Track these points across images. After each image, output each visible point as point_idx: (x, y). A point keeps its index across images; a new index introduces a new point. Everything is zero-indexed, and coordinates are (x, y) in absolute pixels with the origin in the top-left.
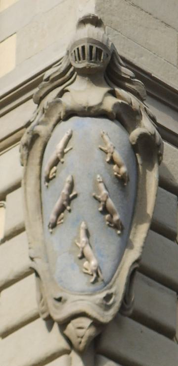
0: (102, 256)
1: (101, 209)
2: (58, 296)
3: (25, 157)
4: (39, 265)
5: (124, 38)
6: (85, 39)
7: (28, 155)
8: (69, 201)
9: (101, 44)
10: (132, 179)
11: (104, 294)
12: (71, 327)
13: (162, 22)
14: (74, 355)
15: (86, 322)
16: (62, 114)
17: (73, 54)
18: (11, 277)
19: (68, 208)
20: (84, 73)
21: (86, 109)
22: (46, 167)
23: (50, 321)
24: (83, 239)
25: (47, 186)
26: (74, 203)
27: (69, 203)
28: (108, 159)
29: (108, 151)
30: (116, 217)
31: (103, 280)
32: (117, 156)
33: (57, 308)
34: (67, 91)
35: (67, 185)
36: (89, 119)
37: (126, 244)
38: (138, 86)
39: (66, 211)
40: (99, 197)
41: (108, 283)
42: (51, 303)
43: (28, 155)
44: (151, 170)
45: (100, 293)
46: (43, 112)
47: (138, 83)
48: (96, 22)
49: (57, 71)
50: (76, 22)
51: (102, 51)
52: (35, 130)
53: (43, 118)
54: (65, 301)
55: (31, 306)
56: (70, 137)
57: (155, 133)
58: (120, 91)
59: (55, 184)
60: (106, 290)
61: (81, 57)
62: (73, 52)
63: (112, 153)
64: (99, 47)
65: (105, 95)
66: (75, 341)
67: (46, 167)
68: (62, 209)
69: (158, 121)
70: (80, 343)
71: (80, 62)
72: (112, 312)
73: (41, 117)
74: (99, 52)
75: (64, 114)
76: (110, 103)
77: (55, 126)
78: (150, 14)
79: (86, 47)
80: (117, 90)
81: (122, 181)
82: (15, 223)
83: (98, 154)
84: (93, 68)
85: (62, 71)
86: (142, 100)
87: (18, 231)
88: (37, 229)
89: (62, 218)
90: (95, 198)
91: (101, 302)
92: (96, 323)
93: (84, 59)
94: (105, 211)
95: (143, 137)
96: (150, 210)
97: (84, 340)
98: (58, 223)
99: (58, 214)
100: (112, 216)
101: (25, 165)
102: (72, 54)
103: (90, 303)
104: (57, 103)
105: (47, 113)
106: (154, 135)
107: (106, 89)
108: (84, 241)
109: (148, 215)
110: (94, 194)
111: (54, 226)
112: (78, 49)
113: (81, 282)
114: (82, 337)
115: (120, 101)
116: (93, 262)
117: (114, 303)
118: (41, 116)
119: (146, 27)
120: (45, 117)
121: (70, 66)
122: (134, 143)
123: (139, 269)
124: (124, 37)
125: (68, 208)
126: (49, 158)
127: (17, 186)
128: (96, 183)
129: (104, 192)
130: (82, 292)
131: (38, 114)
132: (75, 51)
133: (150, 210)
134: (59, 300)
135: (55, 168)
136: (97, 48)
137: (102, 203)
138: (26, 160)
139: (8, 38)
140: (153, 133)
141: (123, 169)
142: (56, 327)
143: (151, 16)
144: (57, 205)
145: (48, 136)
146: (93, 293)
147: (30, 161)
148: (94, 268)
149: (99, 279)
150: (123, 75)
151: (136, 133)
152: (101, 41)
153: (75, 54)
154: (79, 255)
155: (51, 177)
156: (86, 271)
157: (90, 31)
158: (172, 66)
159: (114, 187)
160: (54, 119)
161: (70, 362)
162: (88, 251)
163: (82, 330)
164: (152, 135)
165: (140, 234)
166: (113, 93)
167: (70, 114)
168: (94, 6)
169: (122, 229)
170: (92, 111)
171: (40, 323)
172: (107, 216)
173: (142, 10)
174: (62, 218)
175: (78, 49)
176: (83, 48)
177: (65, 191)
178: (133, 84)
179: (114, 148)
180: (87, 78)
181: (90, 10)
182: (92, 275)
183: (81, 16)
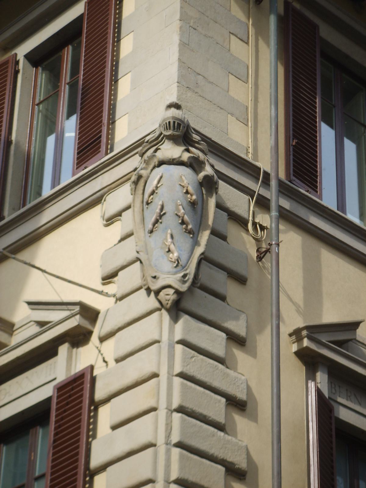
0: (181, 250)
1: (180, 221)
2: (154, 275)
3: (133, 190)
4: (142, 256)
5: (195, 116)
7: (135, 188)
8: (161, 216)
10: (200, 203)
11: (182, 274)
12: (162, 294)
13: (218, 106)
14: (164, 311)
15: (171, 291)
16: (157, 163)
17: (163, 126)
18: (125, 264)
19: (160, 221)
20: (170, 138)
21: (171, 160)
22: (146, 196)
23: (149, 291)
24: (170, 240)
25: (147, 208)
27: (161, 218)
28: (185, 191)
29: (185, 186)
30: (190, 227)
31: (181, 265)
32: (190, 189)
33: (153, 282)
34: (160, 149)
35: (159, 207)
36: (172, 166)
37: (196, 243)
39: (159, 223)
40: (179, 214)
41: (185, 267)
42: (149, 279)
45: (179, 273)
47: (204, 145)
48: (177, 106)
49: (153, 137)
50: (165, 107)
52: (139, 173)
54: (158, 278)
55: (137, 281)
56: (161, 177)
57: (214, 175)
58: (192, 149)
59: (152, 206)
61: (168, 128)
62: (163, 125)
63: (187, 187)
64: (179, 122)
65: (183, 152)
66: (164, 303)
67: (146, 196)
68: (157, 221)
69: (216, 167)
70: (168, 304)
71: (167, 131)
73: (143, 165)
74: (179, 125)
75: (158, 163)
76: (186, 156)
77: (152, 170)
78: (211, 102)
80: (190, 148)
81: (193, 204)
82: (127, 230)
83: (178, 188)
86: (206, 154)
87: (130, 235)
88: (141, 234)
89: (157, 227)
90: (177, 215)
92: (177, 292)
93: (170, 129)
94: (183, 223)
95: (206, 177)
96: (210, 222)
97: (170, 302)
98: (154, 230)
99: (154, 225)
100: (187, 226)
101: (133, 194)
103: (173, 280)
104: (153, 156)
105: (147, 162)
106: (213, 176)
107: (183, 148)
108: (169, 241)
109: (210, 225)
110: (176, 212)
111: (151, 232)
112: (166, 123)
113: (168, 266)
114: (169, 300)
116: (176, 254)
118: (144, 164)
120: (146, 165)
121: (161, 134)
122: (201, 181)
123: (204, 259)
125: (160, 221)
126: (149, 190)
127: (128, 207)
128: (177, 206)
129: (182, 211)
130: (169, 273)
131: (141, 163)
132: (164, 125)
133: (210, 222)
134: (155, 277)
135: (152, 196)
136: (178, 123)
138: (134, 191)
139: (123, 116)
140: (212, 175)
141: (194, 197)
142: (152, 294)
144: (153, 219)
146: (175, 273)
147: (137, 192)
149: (179, 265)
150: (194, 139)
151: (202, 174)
152: (180, 118)
154: (167, 250)
155: (149, 202)
156: (171, 260)
157: (173, 112)
159: (188, 208)
160: (151, 166)
161: (161, 316)
162: (172, 247)
163: (168, 296)
164: (212, 176)
165: (205, 237)
166: (188, 150)
167: (161, 163)
168: (176, 97)
169: (193, 234)
170: (175, 162)
171: (143, 292)
172: (184, 226)
174: (157, 227)
175: (166, 123)
176: (169, 122)
177: (158, 210)
178: (200, 145)
179: (188, 184)
180: (172, 141)
181: (173, 99)
182: (175, 262)
183: (168, 103)
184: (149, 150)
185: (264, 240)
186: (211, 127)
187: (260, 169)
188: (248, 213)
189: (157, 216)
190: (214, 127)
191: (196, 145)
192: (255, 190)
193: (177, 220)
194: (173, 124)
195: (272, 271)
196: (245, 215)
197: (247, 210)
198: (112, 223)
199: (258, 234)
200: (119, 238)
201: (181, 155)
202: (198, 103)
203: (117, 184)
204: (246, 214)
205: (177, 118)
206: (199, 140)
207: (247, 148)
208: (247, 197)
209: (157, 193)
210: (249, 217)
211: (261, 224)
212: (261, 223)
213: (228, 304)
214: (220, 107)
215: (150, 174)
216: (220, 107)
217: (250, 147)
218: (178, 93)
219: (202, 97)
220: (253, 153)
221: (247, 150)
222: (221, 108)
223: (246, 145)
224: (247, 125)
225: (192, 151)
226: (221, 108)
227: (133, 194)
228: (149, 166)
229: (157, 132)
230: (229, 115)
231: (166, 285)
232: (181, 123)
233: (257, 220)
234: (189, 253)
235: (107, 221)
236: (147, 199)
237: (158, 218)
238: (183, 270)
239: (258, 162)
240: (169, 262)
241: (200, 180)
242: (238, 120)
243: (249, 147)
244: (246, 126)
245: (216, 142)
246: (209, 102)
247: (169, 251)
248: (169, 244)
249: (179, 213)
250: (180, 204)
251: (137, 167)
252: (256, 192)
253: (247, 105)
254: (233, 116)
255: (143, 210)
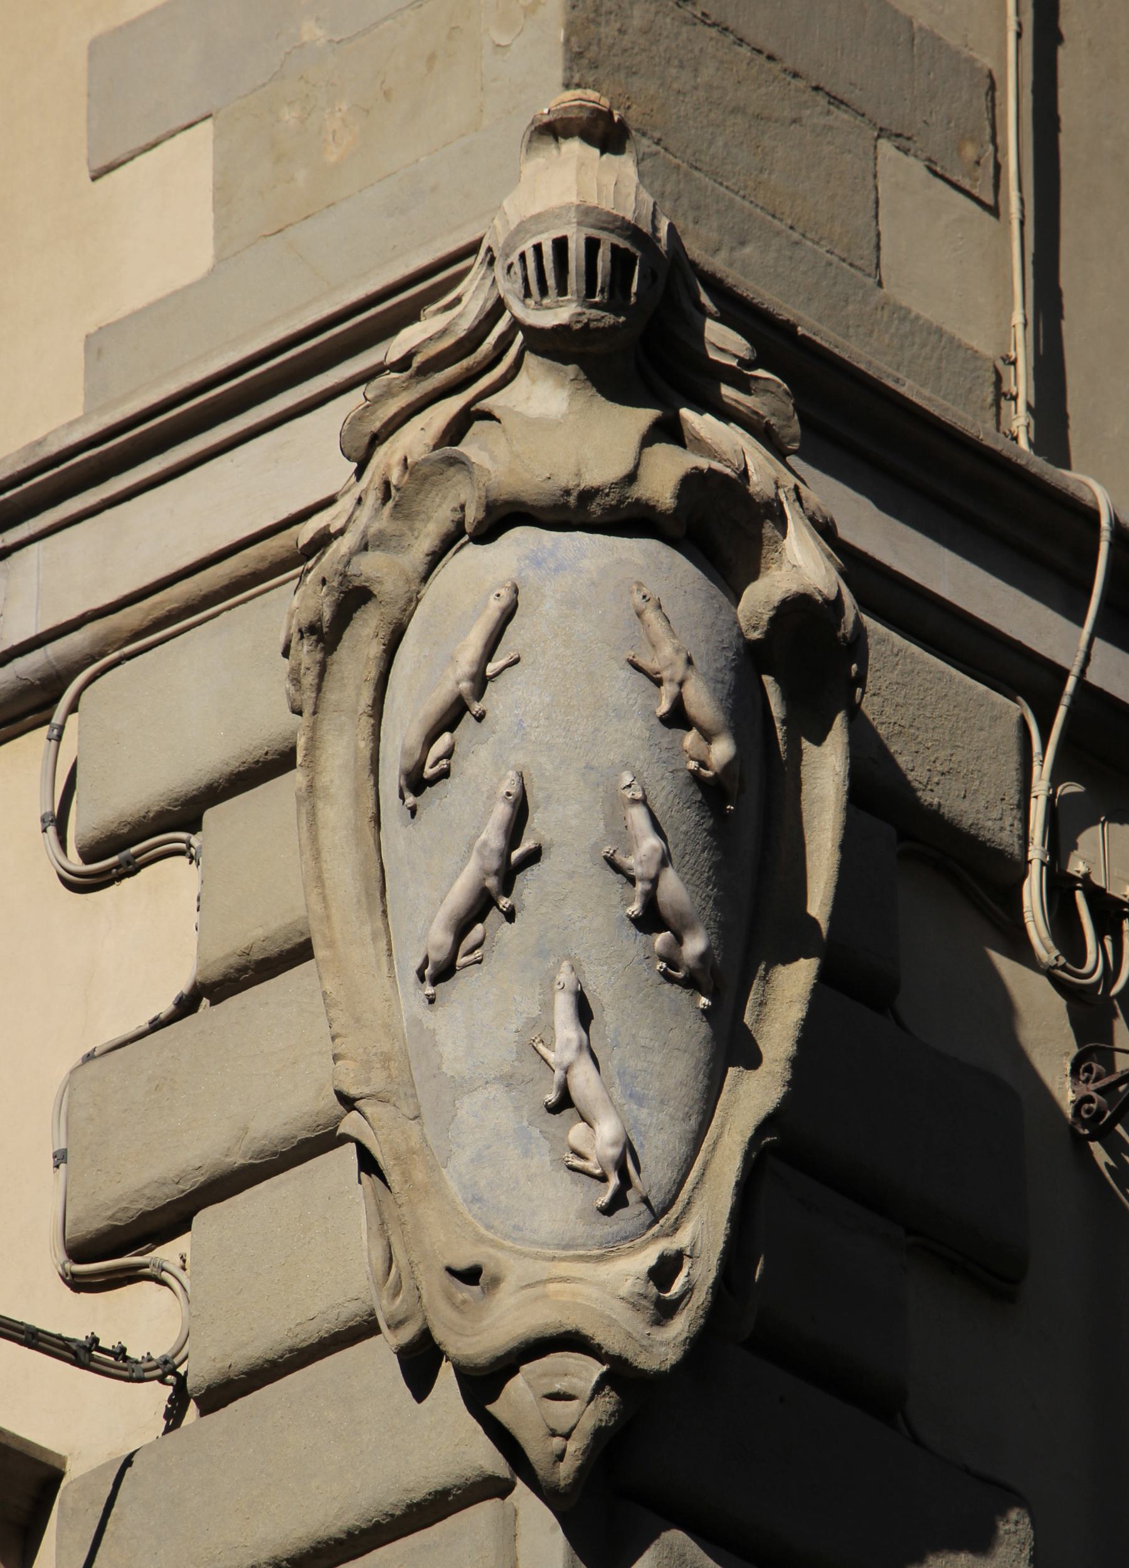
0: (640, 1100)
1: (635, 908)
2: (462, 1264)
3: (309, 679)
5: (678, 167)
6: (567, 207)
7: (323, 670)
9: (631, 231)
11: (649, 1257)
13: (817, 88)
16: (473, 515)
17: (517, 268)
18: (238, 1159)
19: (504, 902)
21: (572, 500)
24: (567, 1030)
25: (413, 811)
26: (528, 884)
27: (507, 887)
28: (664, 707)
29: (665, 674)
31: (645, 1201)
33: (459, 1307)
34: (488, 416)
35: (502, 812)
36: (581, 537)
38: (767, 398)
39: (494, 915)
40: (630, 862)
41: (665, 1210)
43: (323, 670)
44: (818, 739)
45: (633, 1250)
46: (386, 496)
47: (773, 388)
49: (443, 333)
50: (522, 125)
51: (633, 258)
52: (351, 571)
53: (384, 522)
54: (496, 1281)
56: (508, 614)
57: (839, 592)
60: (656, 1237)
61: (551, 281)
62: (514, 258)
63: (681, 684)
64: (623, 244)
65: (648, 440)
66: (537, 1449)
69: (844, 533)
70: (561, 1457)
71: (546, 301)
72: (681, 1326)
74: (622, 261)
75: (481, 515)
77: (436, 558)
78: (771, 58)
79: (572, 245)
84: (597, 329)
85: (462, 334)
86: (780, 452)
89: (479, 945)
90: (612, 864)
91: (640, 1288)
93: (562, 290)
97: (575, 1446)
98: (461, 961)
99: (462, 928)
100: (679, 940)
101: (308, 710)
102: (510, 266)
106: (838, 601)
108: (569, 1041)
109: (814, 922)
110: (608, 849)
111: (445, 972)
112: (538, 248)
114: (567, 1436)
115: (704, 463)
117: (688, 1291)
118: (377, 511)
119: (758, 117)
120: (393, 516)
121: (499, 307)
122: (755, 635)
124: (678, 161)
125: (504, 902)
129: (650, 843)
131: (360, 501)
132: (522, 256)
134: (471, 1276)
135: (445, 739)
136: (615, 248)
137: (640, 887)
139: (172, 135)
140: (832, 596)
142: (446, 1379)
143: (776, 67)
145: (410, 600)
146: (609, 1250)
147: (332, 696)
148: (614, 1152)
149: (631, 1196)
150: (713, 355)
152: (629, 216)
153: (525, 268)
154: (552, 1097)
155: (428, 772)
156: (577, 1163)
158: (859, 274)
164: (826, 600)
168: (561, 35)
170: (595, 508)
172: (661, 939)
173: (741, 41)
174: (479, 945)
175: (538, 248)
176: (561, 245)
177: (492, 836)
178: (747, 391)
179: (689, 661)
180: (572, 369)
182: (603, 1178)
184: (418, 421)
185: (1119, 996)
186: (778, 233)
187: (1091, 516)
188: (1017, 814)
189: (487, 874)
190: (796, 236)
191: (728, 392)
192: (1061, 660)
193: (616, 899)
194: (583, 263)
195: (293, 578)
196: (1002, 829)
197: (1013, 796)
198: (130, 869)
199: (1081, 961)
200: (182, 985)
201: (637, 466)
202: (696, 70)
203: (158, 613)
204: (1008, 821)
205: (608, 213)
206: (742, 361)
207: (1000, 364)
208: (1020, 709)
209: (480, 718)
210: (1025, 839)
211: (1103, 885)
212: (1099, 880)
213: (916, 1441)
214: (828, 94)
215: (425, 579)
216: (828, 94)
217: (1021, 364)
218: (574, 7)
219: (714, 25)
220: (1032, 403)
221: (999, 380)
222: (836, 101)
223: (989, 351)
224: (994, 210)
225: (704, 433)
226: (836, 101)
227: (308, 710)
228: (412, 529)
229: (465, 300)
230: (886, 147)
231: (550, 1331)
232: (633, 250)
233: (1077, 866)
234: (688, 1116)
235: (88, 855)
236: (417, 756)
237: (492, 883)
238: (656, 1228)
239: (1068, 466)
240: (568, 1175)
241: (755, 628)
242: (942, 177)
243: (1014, 363)
244: (986, 216)
245: (826, 345)
246: (762, 58)
247: (564, 1102)
248: (568, 1056)
249: (629, 853)
250: (639, 795)
251: (332, 530)
252: (1064, 673)
253: (987, 62)
254: (906, 152)
255: (377, 820)
